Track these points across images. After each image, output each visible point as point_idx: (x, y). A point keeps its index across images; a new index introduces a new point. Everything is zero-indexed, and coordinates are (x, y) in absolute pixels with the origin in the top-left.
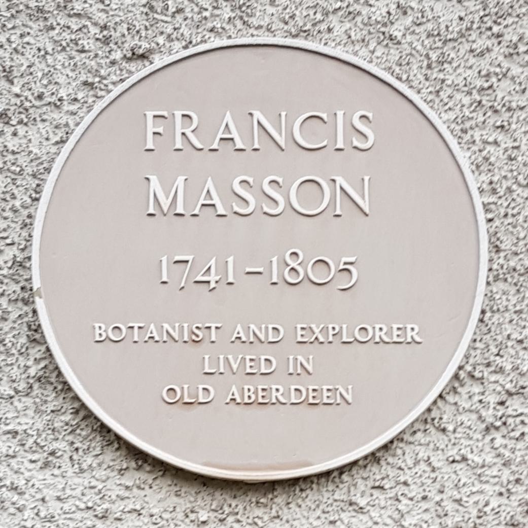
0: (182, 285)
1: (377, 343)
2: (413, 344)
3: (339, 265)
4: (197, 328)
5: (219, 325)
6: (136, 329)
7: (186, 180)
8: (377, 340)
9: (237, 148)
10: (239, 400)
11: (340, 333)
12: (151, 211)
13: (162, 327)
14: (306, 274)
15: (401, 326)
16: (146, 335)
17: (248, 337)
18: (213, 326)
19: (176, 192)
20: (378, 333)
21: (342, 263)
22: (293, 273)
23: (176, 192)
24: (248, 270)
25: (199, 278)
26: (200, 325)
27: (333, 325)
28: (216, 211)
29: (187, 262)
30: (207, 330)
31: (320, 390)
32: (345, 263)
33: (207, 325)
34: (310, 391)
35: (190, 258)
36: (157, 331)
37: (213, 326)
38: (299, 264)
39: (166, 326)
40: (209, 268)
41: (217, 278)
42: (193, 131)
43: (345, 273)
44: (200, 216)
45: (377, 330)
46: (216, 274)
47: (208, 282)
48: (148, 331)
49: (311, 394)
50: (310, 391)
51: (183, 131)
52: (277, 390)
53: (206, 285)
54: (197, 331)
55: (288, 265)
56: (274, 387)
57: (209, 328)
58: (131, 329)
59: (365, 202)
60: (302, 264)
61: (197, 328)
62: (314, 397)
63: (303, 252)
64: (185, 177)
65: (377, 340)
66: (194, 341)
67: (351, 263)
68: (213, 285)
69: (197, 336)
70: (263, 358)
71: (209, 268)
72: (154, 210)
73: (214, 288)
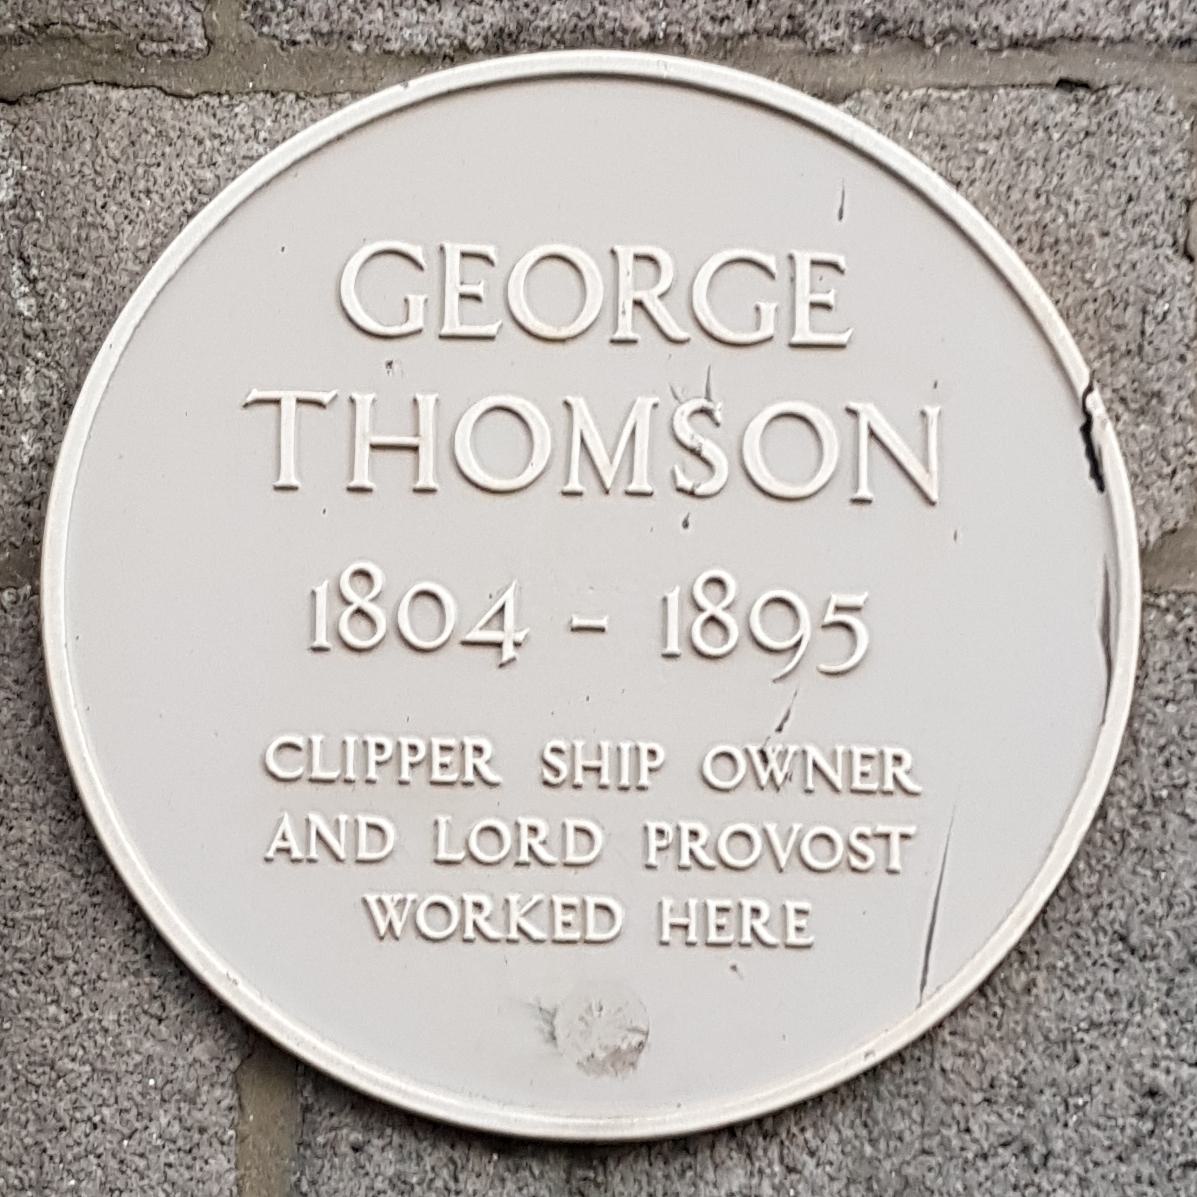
3: (823, 615)
4: (861, 836)
5: (910, 830)
7: (655, 406)
8: (525, 856)
10: (297, 853)
12: (574, 485)
13: (308, 821)
15: (872, 751)
17: (308, 850)
18: (896, 832)
19: (633, 432)
21: (831, 608)
22: (714, 630)
23: (633, 432)
24: (577, 622)
25: (477, 635)
26: (867, 831)
30: (881, 842)
32: (839, 609)
33: (882, 829)
34: (712, 912)
37: (896, 832)
41: (520, 637)
42: (661, 296)
43: (842, 634)
46: (518, 629)
47: (499, 645)
51: (639, 295)
53: (492, 652)
54: (859, 845)
55: (700, 609)
57: (887, 836)
59: (931, 477)
61: (861, 836)
62: (720, 928)
63: (381, 567)
64: (656, 400)
66: (854, 870)
67: (855, 609)
68: (509, 651)
69: (864, 857)
70: (591, 901)
72: (581, 482)
73: (513, 660)
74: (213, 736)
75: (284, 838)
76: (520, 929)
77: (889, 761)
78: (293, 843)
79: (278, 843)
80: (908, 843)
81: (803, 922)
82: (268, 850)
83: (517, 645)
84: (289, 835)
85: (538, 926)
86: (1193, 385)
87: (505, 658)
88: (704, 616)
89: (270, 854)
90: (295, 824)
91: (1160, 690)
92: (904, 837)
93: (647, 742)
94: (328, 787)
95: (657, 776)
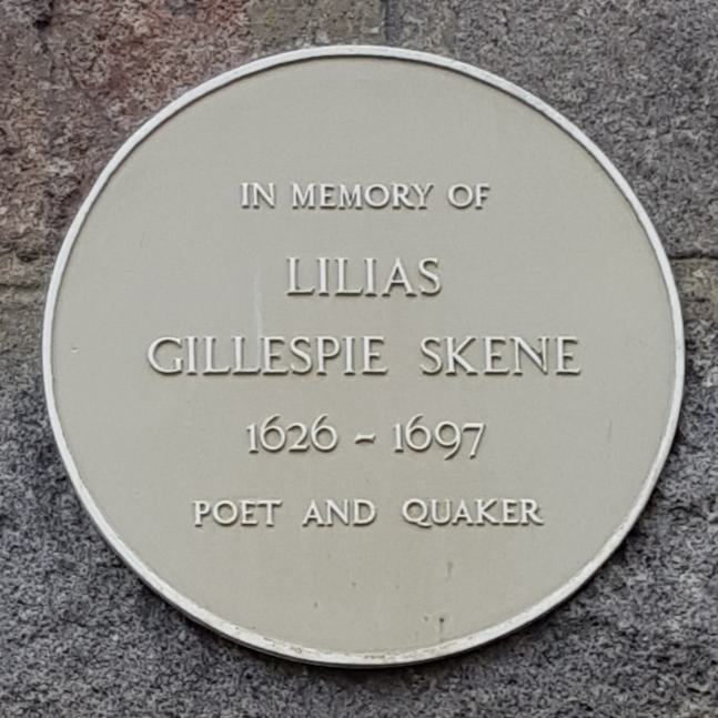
0: (473, 453)
1: (396, 208)
2: (366, 210)
5: (278, 502)
6: (269, 507)
8: (396, 203)
11: (342, 354)
14: (433, 439)
16: (304, 516)
17: (325, 520)
18: (269, 503)
20: (396, 195)
25: (296, 446)
27: (529, 501)
28: (406, 290)
29: (477, 429)
31: (508, 342)
33: (262, 502)
34: (244, 508)
35: (480, 425)
36: (469, 510)
39: (330, 503)
44: (492, 188)
45: (396, 190)
48: (468, 507)
49: (245, 512)
50: (244, 508)
52: (529, 505)
56: (524, 501)
58: (262, 509)
65: (396, 203)
74: (423, 621)
75: (462, 512)
76: (484, 518)
77: (524, 506)
78: (317, 516)
79: (308, 516)
80: (276, 510)
81: (511, 511)
82: (195, 519)
84: (465, 511)
85: (493, 516)
86: (182, 716)
89: (198, 521)
90: (467, 505)
91: (17, 84)
92: (274, 506)
93: (525, 498)
94: (253, 378)
95: (541, 513)
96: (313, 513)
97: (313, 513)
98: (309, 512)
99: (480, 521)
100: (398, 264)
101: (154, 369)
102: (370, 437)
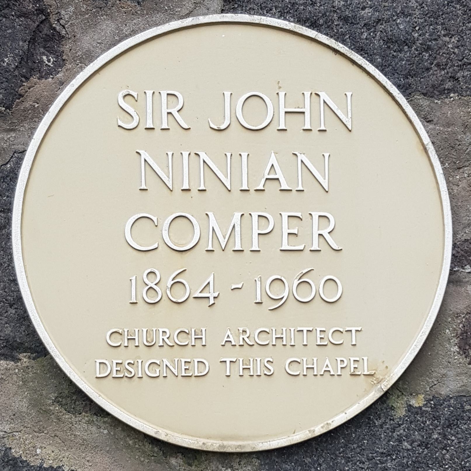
5: (359, 329)
8: (161, 344)
9: (282, 188)
14: (318, 292)
25: (198, 295)
37: (354, 329)
38: (156, 284)
40: (209, 283)
41: (216, 295)
47: (208, 298)
53: (207, 300)
55: (147, 285)
60: (159, 284)
69: (131, 372)
71: (209, 283)
80: (358, 333)
83: (215, 298)
87: (211, 303)
88: (148, 287)
96: (228, 336)
97: (228, 336)
98: (325, 365)
99: (241, 343)
100: (229, 333)
101: (146, 302)
102: (240, 286)
